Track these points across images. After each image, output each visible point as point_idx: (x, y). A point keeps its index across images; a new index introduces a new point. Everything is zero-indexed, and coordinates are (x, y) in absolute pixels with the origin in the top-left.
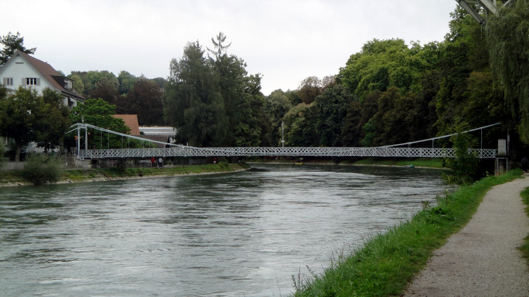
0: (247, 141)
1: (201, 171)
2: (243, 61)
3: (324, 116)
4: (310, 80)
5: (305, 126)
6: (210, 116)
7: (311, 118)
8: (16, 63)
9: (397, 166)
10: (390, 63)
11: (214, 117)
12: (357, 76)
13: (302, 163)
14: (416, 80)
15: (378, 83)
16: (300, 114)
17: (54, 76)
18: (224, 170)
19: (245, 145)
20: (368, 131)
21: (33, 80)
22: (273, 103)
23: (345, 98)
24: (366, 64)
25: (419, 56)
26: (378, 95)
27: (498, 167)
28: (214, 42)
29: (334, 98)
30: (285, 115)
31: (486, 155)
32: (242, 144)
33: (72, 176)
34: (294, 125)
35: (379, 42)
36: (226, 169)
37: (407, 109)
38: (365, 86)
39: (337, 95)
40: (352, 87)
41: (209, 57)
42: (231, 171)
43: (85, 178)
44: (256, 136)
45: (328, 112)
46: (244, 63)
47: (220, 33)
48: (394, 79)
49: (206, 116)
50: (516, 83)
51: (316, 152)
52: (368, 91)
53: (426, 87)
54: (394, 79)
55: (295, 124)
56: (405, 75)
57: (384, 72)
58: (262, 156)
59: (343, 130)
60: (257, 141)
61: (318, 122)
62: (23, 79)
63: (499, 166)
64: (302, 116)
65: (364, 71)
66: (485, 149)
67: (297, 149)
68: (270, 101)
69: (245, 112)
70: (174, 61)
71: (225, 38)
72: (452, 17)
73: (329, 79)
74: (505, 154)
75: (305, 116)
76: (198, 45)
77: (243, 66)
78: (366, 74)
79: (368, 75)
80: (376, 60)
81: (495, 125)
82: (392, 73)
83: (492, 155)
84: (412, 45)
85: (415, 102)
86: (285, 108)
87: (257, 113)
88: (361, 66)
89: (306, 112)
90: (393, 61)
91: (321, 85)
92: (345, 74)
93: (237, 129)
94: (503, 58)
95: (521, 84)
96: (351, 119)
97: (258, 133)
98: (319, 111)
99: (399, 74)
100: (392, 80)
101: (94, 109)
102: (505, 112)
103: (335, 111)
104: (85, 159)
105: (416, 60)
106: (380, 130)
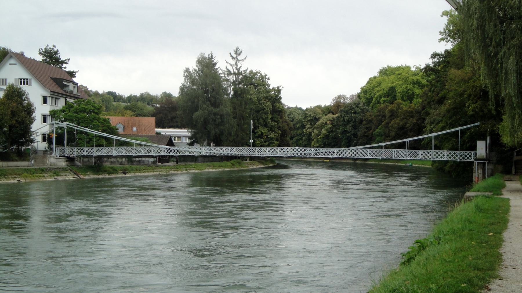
0: (265, 142)
1: (205, 169)
2: (266, 75)
3: (346, 124)
4: (340, 97)
5: (332, 131)
6: (218, 118)
7: (336, 125)
8: (10, 64)
9: (399, 164)
10: (397, 82)
11: (221, 119)
12: (373, 93)
13: (329, 160)
14: (418, 95)
15: (388, 99)
16: (328, 122)
17: (56, 78)
18: (235, 167)
19: (263, 145)
20: (378, 136)
21: (26, 81)
22: (309, 114)
23: (361, 109)
24: (380, 84)
25: (420, 76)
26: (386, 108)
27: (476, 171)
28: (231, 56)
29: (353, 110)
30: (317, 123)
31: (463, 158)
32: (260, 144)
33: (25, 174)
34: (323, 130)
35: (391, 68)
36: (238, 166)
37: (408, 118)
38: (378, 101)
39: (355, 107)
40: (369, 102)
41: (227, 68)
42: (244, 167)
43: (44, 176)
44: (273, 138)
45: (349, 120)
46: (267, 77)
47: (237, 48)
48: (400, 95)
49: (214, 118)
50: (496, 54)
51: (221, 152)
52: (380, 104)
53: (424, 100)
54: (400, 95)
55: (324, 130)
56: (409, 92)
57: (393, 89)
58: (187, 156)
59: (359, 135)
60: (273, 142)
61: (341, 128)
62: (16, 79)
63: (477, 170)
64: (330, 124)
65: (377, 89)
66: (463, 152)
67: (297, 149)
68: (306, 112)
69: (264, 117)
70: (187, 70)
71: (241, 52)
72: (441, 35)
73: (355, 97)
74: (485, 157)
75: (332, 124)
76: (212, 56)
77: (266, 80)
78: (379, 91)
79: (381, 92)
80: (387, 81)
81: (474, 126)
82: (399, 90)
83: (470, 158)
84: (414, 68)
85: (414, 112)
86: (318, 118)
87: (278, 119)
88: (376, 86)
89: (332, 121)
90: (400, 81)
91: (348, 101)
92: (364, 92)
93: (257, 132)
94: (477, 16)
95: (504, 53)
96: (366, 126)
97: (275, 135)
98: (341, 120)
99: (404, 91)
100: (399, 95)
101: (79, 108)
102: (484, 110)
103: (353, 120)
104: (60, 156)
105: (418, 80)
106: (387, 135)
